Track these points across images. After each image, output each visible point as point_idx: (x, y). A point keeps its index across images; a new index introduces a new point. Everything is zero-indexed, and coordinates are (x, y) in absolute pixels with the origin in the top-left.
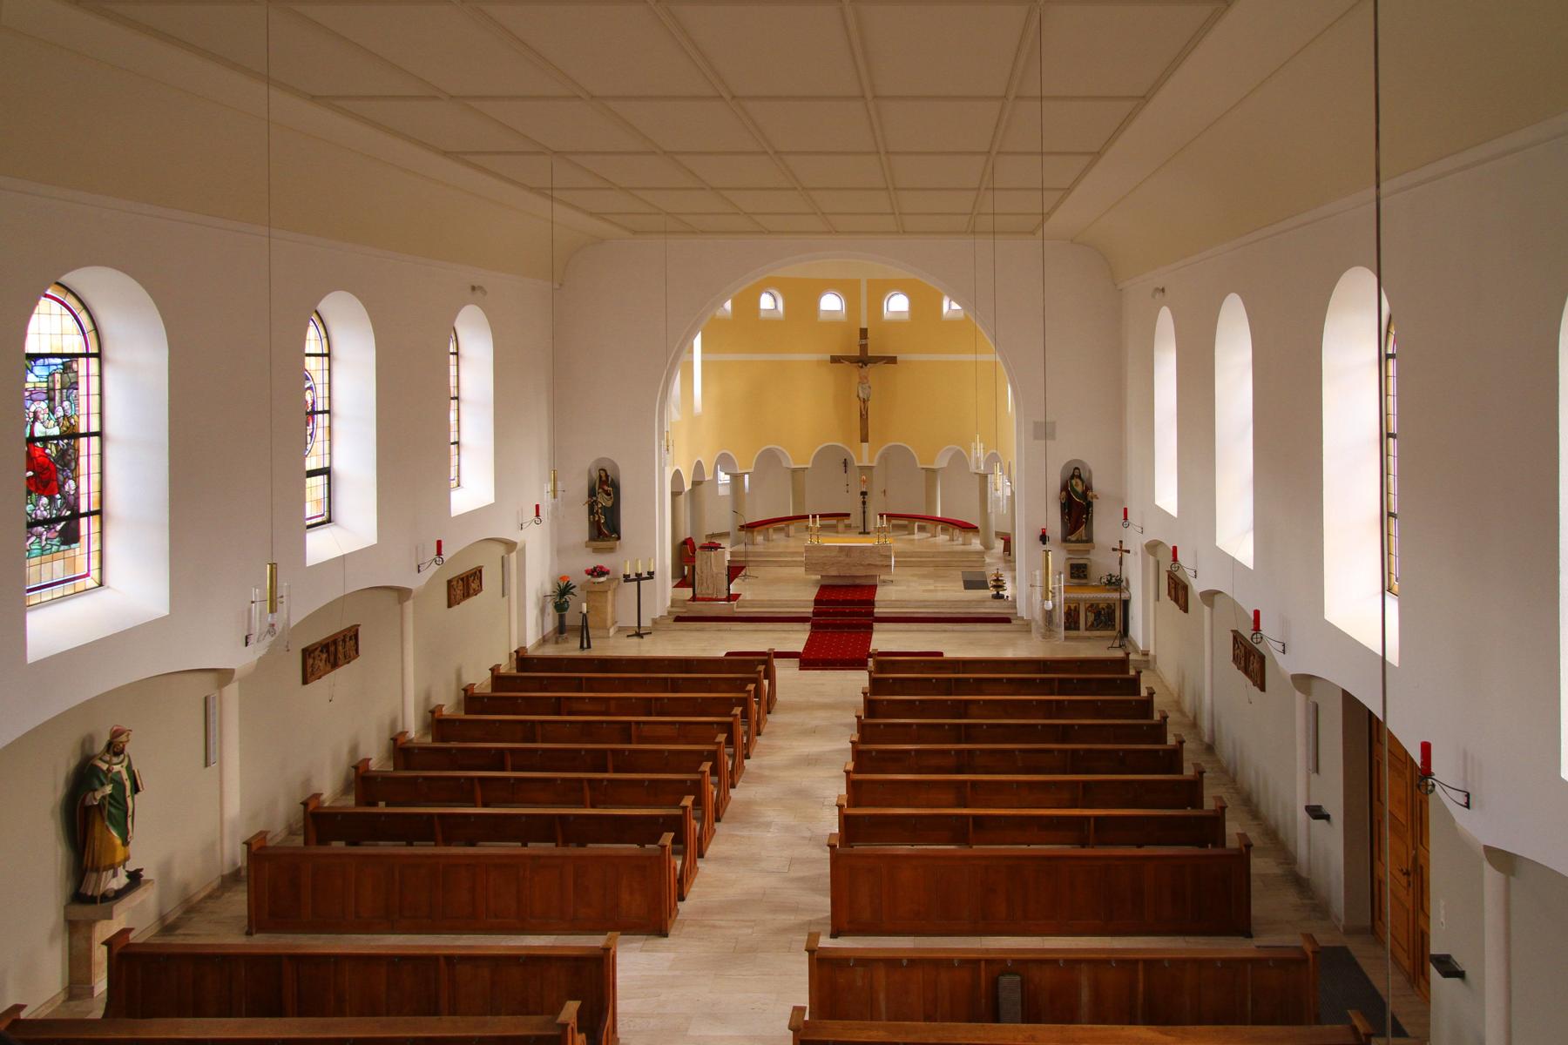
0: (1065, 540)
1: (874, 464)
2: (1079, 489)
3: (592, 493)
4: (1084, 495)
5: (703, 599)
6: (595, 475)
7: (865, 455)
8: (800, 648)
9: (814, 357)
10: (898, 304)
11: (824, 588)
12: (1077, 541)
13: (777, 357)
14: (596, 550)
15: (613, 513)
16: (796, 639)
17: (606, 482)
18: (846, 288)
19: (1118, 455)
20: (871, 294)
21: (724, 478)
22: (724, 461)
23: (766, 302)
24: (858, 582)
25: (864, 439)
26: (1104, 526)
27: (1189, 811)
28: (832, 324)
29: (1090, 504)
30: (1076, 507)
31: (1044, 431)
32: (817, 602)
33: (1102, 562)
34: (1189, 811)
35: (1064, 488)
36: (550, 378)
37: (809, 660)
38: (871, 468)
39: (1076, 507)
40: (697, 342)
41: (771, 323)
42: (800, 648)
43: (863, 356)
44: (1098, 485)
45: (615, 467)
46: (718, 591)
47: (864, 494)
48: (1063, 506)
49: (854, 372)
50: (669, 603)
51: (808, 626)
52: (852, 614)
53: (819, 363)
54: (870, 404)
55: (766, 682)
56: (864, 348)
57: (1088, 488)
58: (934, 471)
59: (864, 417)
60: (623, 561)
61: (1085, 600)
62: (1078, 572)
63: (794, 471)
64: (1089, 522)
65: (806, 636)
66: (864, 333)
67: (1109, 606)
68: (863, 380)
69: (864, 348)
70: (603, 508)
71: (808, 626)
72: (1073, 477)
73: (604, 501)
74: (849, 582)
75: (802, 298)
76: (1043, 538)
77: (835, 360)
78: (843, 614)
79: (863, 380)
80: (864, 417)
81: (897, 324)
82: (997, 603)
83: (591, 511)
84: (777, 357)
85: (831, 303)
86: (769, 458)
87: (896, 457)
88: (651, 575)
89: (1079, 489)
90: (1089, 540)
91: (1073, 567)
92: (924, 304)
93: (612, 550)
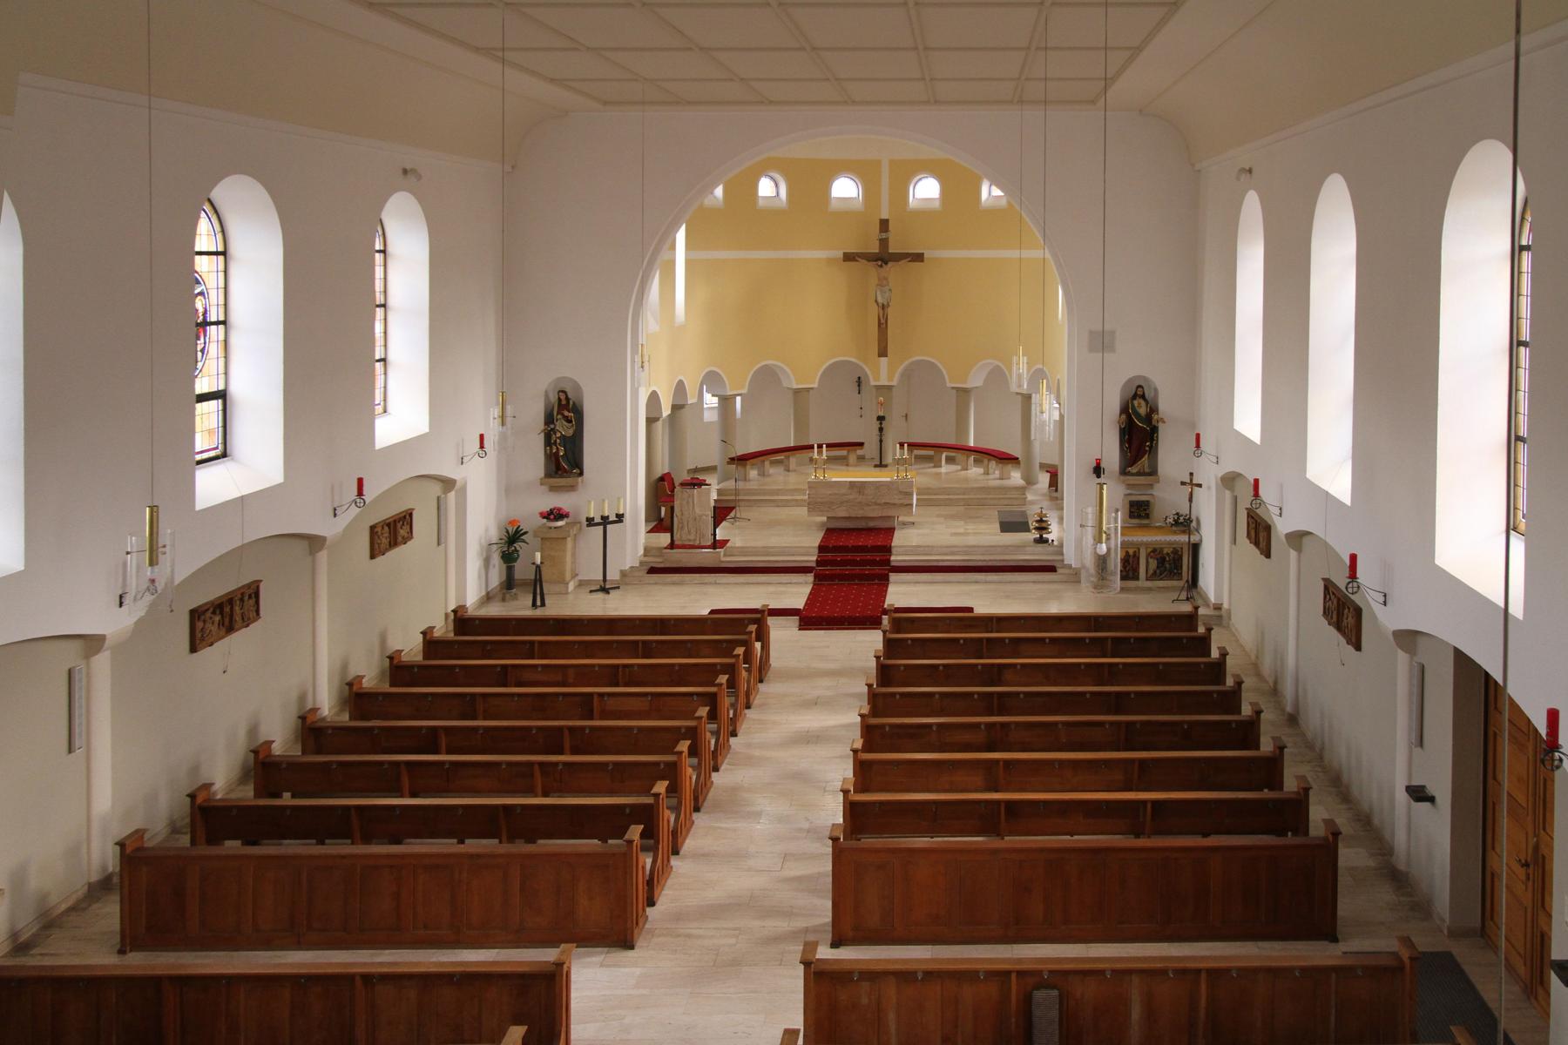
1: (894, 383)
2: (1143, 411)
3: (549, 419)
4: (1148, 418)
6: (553, 398)
7: (882, 373)
8: (801, 606)
10: (926, 190)
11: (830, 532)
12: (1139, 474)
13: (780, 254)
14: (553, 489)
16: (796, 593)
17: (566, 406)
18: (863, 171)
19: (1191, 371)
20: (887, 179)
21: (710, 401)
22: (711, 380)
23: (766, 188)
24: (872, 524)
25: (883, 353)
26: (1171, 456)
28: (846, 215)
29: (1155, 430)
30: (1139, 432)
31: (1101, 342)
32: (821, 549)
33: (1168, 499)
34: (1266, 794)
35: (1125, 410)
36: (495, 280)
37: (810, 619)
38: (890, 388)
39: (1139, 432)
40: (681, 236)
41: (771, 214)
42: (801, 606)
43: (883, 253)
44: (1163, 406)
45: (578, 388)
46: (703, 536)
48: (1122, 432)
49: (872, 270)
51: (810, 578)
53: (830, 261)
54: (890, 311)
55: (758, 645)
56: (884, 243)
57: (1153, 410)
59: (883, 326)
60: (584, 501)
61: (1147, 545)
62: (1139, 511)
63: (797, 392)
64: (1153, 450)
65: (807, 590)
66: (884, 224)
67: (1175, 551)
68: (882, 283)
69: (884, 243)
70: (563, 437)
71: (810, 578)
72: (1135, 396)
73: (564, 429)
75: (809, 182)
76: (1098, 470)
77: (849, 257)
78: (853, 563)
79: (882, 283)
80: (883, 326)
81: (925, 214)
82: (1040, 548)
84: (780, 254)
86: (766, 378)
87: (921, 375)
88: (620, 518)
89: (1143, 411)
90: (1153, 472)
91: (1132, 504)
92: (959, 188)
93: (572, 488)
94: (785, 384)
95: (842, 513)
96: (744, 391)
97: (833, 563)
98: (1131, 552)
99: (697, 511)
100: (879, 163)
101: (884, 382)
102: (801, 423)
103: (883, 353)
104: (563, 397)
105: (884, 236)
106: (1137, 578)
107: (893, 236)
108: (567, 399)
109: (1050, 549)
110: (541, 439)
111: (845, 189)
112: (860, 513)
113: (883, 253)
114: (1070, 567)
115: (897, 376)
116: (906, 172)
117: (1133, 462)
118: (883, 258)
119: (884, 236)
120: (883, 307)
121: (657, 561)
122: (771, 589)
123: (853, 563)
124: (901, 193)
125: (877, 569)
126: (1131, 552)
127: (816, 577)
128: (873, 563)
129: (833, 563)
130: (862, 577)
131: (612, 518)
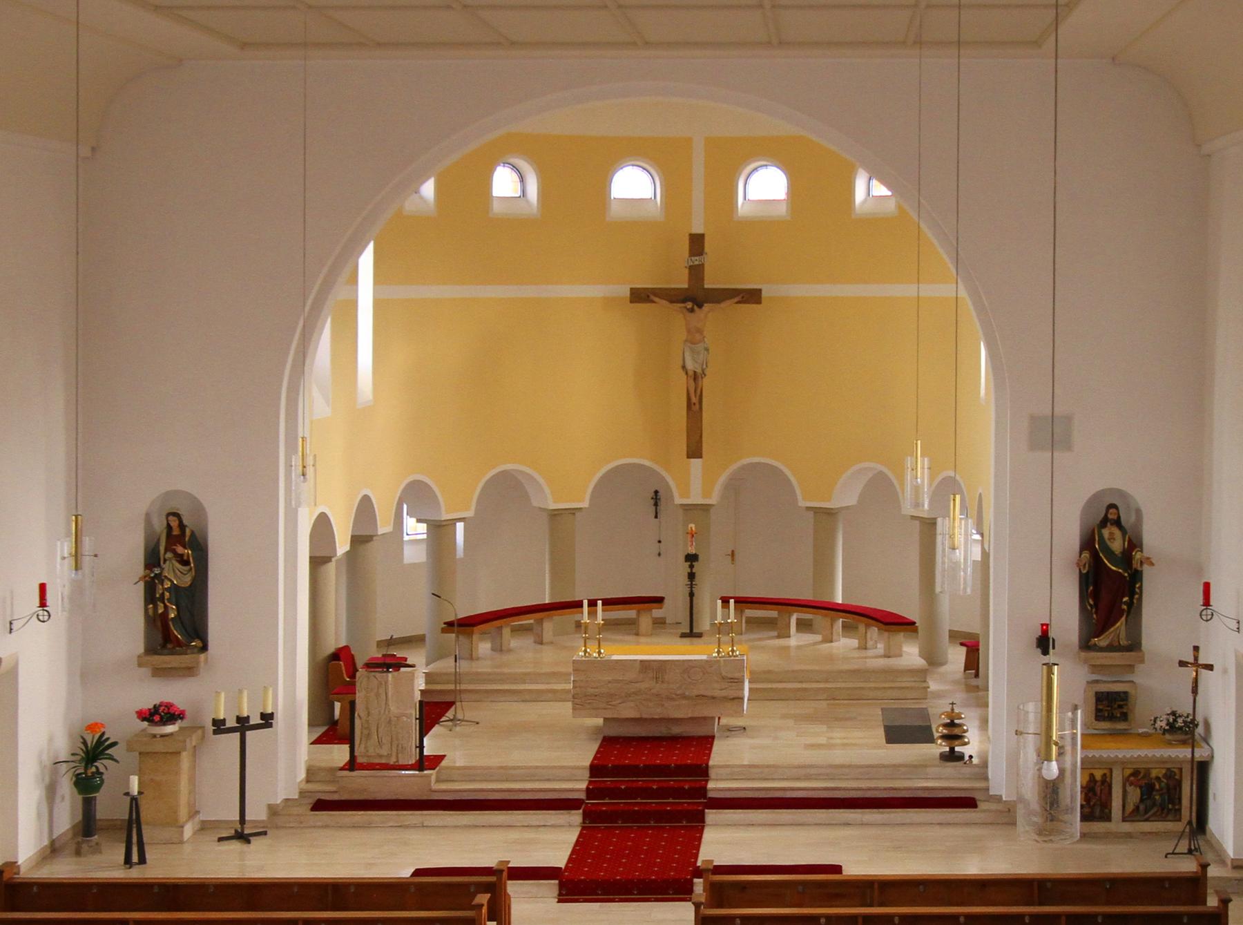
0: (1086, 645)
2: (1117, 546)
3: (152, 560)
4: (1126, 558)
6: (159, 525)
7: (694, 484)
10: (766, 186)
11: (609, 743)
12: (1111, 648)
14: (159, 672)
15: (193, 601)
18: (661, 156)
19: (1194, 482)
21: (415, 529)
22: (416, 496)
23: (504, 183)
24: (676, 730)
25: (695, 451)
26: (1163, 619)
28: (634, 225)
29: (1136, 576)
31: (1049, 433)
33: (1157, 688)
35: (1089, 543)
37: (575, 884)
38: (705, 508)
41: (514, 226)
43: (695, 289)
44: (1153, 538)
45: (199, 510)
47: (691, 558)
48: (1084, 580)
49: (677, 319)
53: (609, 302)
54: (706, 383)
56: (696, 272)
57: (1134, 544)
58: (830, 513)
59: (694, 408)
60: (210, 692)
61: (1123, 763)
62: (1111, 708)
63: (555, 515)
64: (1134, 609)
65: (572, 836)
66: (697, 243)
68: (694, 337)
69: (696, 272)
70: (175, 589)
71: (576, 817)
72: (1104, 522)
73: (175, 575)
75: (575, 174)
76: (1044, 642)
77: (639, 296)
78: (646, 792)
79: (694, 337)
80: (694, 408)
81: (763, 226)
82: (950, 768)
83: (151, 596)
84: (529, 291)
85: (633, 184)
86: (506, 492)
87: (758, 487)
88: (267, 720)
89: (1117, 546)
90: (1134, 645)
92: (817, 185)
93: (190, 671)
94: (536, 503)
95: (628, 711)
96: (470, 514)
97: (613, 792)
98: (1098, 775)
101: (696, 498)
102: (561, 565)
104: (174, 523)
105: (696, 261)
106: (1108, 818)
107: (710, 260)
108: (182, 527)
109: (967, 770)
110: (135, 596)
113: (695, 289)
114: (998, 799)
116: (731, 160)
117: (1101, 629)
118: (695, 297)
119: (696, 261)
120: (695, 377)
122: (513, 835)
123: (646, 792)
124: (724, 189)
126: (1098, 775)
127: (586, 816)
128: (678, 793)
129: (613, 792)
130: (661, 816)
131: (255, 720)
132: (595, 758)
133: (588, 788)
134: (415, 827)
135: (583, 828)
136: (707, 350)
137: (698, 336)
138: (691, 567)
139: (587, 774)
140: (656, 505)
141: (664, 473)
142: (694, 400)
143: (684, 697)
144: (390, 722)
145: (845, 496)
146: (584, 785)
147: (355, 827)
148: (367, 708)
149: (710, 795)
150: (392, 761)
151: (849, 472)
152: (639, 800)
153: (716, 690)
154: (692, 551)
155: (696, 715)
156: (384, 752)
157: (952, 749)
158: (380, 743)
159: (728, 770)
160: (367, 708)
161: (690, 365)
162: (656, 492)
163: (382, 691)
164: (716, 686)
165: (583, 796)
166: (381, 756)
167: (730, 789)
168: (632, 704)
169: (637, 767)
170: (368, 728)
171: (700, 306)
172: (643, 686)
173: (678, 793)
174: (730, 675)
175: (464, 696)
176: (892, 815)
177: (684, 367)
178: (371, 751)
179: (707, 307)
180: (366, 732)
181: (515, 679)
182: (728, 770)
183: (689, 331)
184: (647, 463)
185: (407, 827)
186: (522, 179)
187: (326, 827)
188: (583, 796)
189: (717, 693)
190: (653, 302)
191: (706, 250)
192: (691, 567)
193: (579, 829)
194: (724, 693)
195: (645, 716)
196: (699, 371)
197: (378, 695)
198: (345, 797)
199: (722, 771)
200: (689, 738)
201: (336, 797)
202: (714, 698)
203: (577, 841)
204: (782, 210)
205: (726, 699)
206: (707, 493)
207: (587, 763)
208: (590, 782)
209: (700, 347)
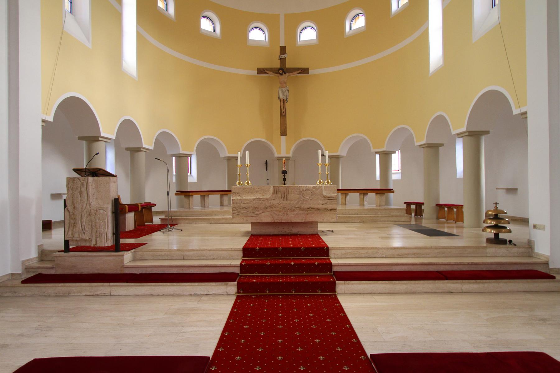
1: (290, 155)
5: (79, 249)
7: (283, 148)
9: (244, 72)
10: (308, 35)
11: (253, 237)
18: (270, 22)
23: (206, 25)
24: (295, 230)
25: (284, 133)
27: (151, 223)
28: (257, 47)
32: (247, 251)
34: (151, 223)
38: (288, 159)
41: (207, 37)
43: (283, 70)
46: (99, 235)
47: (284, 172)
50: (33, 254)
51: (232, 288)
52: (274, 268)
53: (249, 77)
54: (287, 105)
56: (283, 61)
59: (283, 115)
66: (283, 50)
69: (283, 61)
71: (232, 288)
74: (285, 230)
75: (236, 23)
77: (261, 71)
78: (286, 268)
80: (283, 115)
81: (308, 47)
82: (501, 249)
92: (330, 22)
94: (222, 155)
95: (266, 219)
97: (261, 268)
99: (94, 203)
100: (278, 16)
101: (283, 154)
102: (232, 177)
103: (284, 133)
109: (514, 250)
111: (257, 35)
112: (284, 219)
113: (283, 70)
115: (291, 151)
116: (294, 22)
118: (282, 70)
119: (283, 56)
121: (48, 269)
122: (178, 304)
123: (286, 268)
124: (292, 34)
125: (319, 276)
127: (239, 287)
128: (311, 268)
129: (261, 268)
130: (300, 287)
132: (246, 244)
133: (241, 264)
134: (105, 295)
135: (238, 297)
136: (288, 90)
137: (284, 85)
138: (284, 176)
139: (241, 254)
140: (266, 166)
141: (271, 144)
142: (283, 111)
143: (300, 209)
144: (90, 214)
145: (342, 151)
146: (238, 262)
147: (57, 296)
148: (73, 203)
149: (335, 269)
150: (93, 244)
151: (345, 140)
152: (256, 274)
153: (319, 204)
154: (284, 169)
155: (308, 220)
156: (86, 237)
157: (496, 235)
158: (83, 230)
159: (343, 251)
160: (73, 203)
161: (281, 96)
162: (266, 161)
163: (84, 189)
164: (321, 202)
165: (238, 270)
166: (86, 240)
167: (349, 265)
168: (268, 213)
169: (276, 249)
170: (75, 219)
171: (285, 73)
172: (275, 202)
173: (311, 268)
174: (328, 195)
175: (180, 222)
176: (486, 285)
177: (279, 98)
178: (77, 237)
179: (287, 74)
180: (73, 222)
181: (208, 215)
182: (343, 251)
183: (281, 83)
184: (264, 140)
185: (98, 296)
186: (214, 26)
187: (34, 296)
188: (238, 270)
189: (320, 206)
190: (268, 74)
191: (287, 52)
192: (284, 176)
193: (234, 298)
194: (325, 206)
195: (276, 221)
196: (285, 99)
197: (81, 193)
198: (60, 272)
199: (338, 252)
200: (305, 235)
201: (52, 272)
202: (318, 209)
203: (232, 312)
204: (315, 42)
205: (326, 210)
206: (288, 152)
207: (241, 246)
208: (243, 261)
209: (286, 89)
